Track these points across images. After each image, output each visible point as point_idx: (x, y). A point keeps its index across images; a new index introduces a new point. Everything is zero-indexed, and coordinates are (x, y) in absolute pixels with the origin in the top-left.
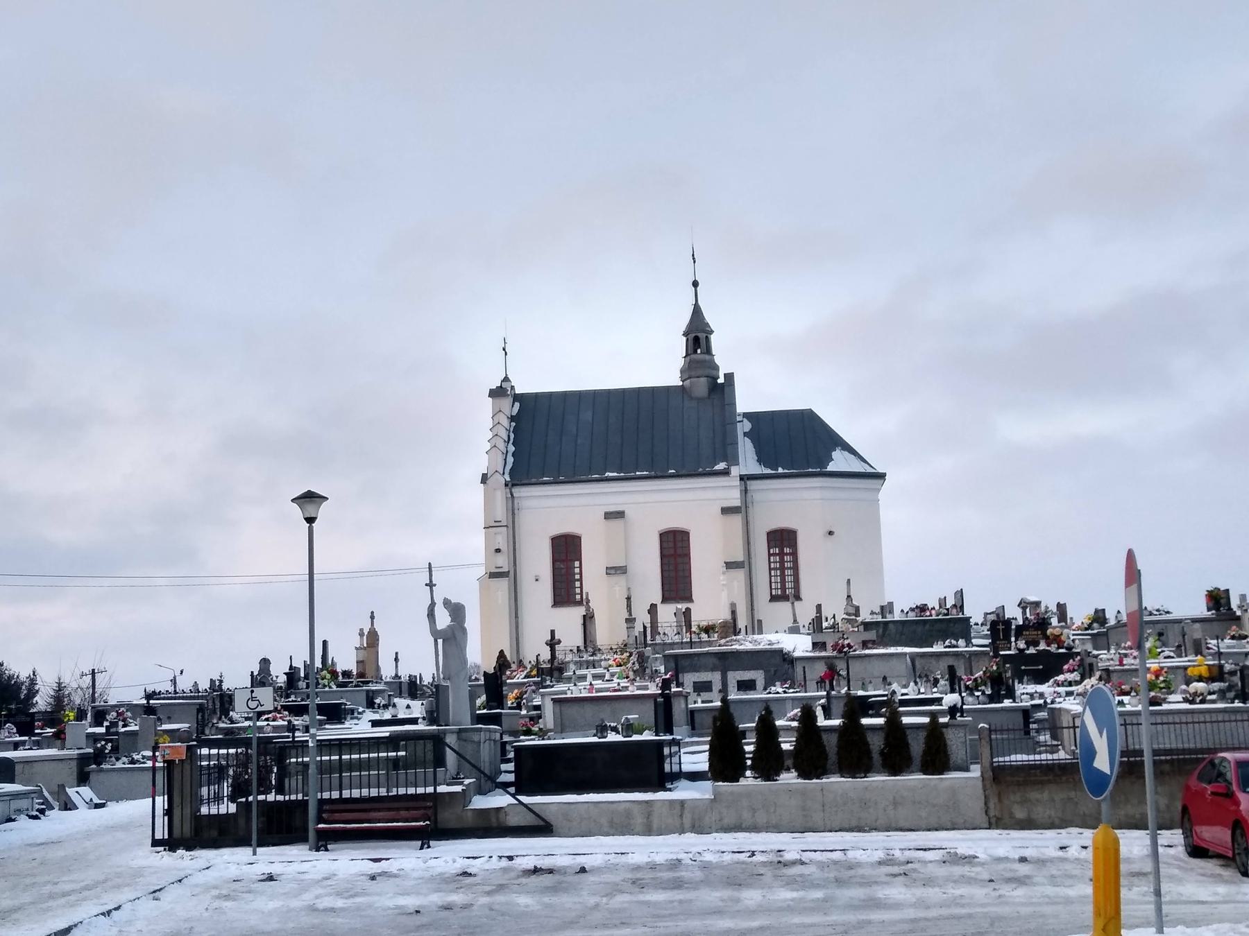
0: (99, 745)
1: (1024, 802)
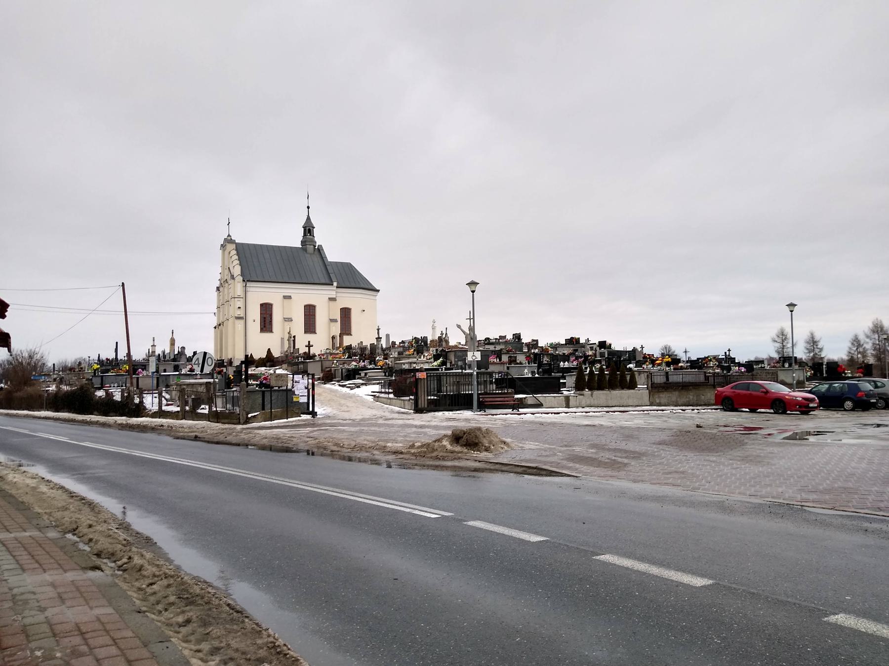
1: (659, 397)
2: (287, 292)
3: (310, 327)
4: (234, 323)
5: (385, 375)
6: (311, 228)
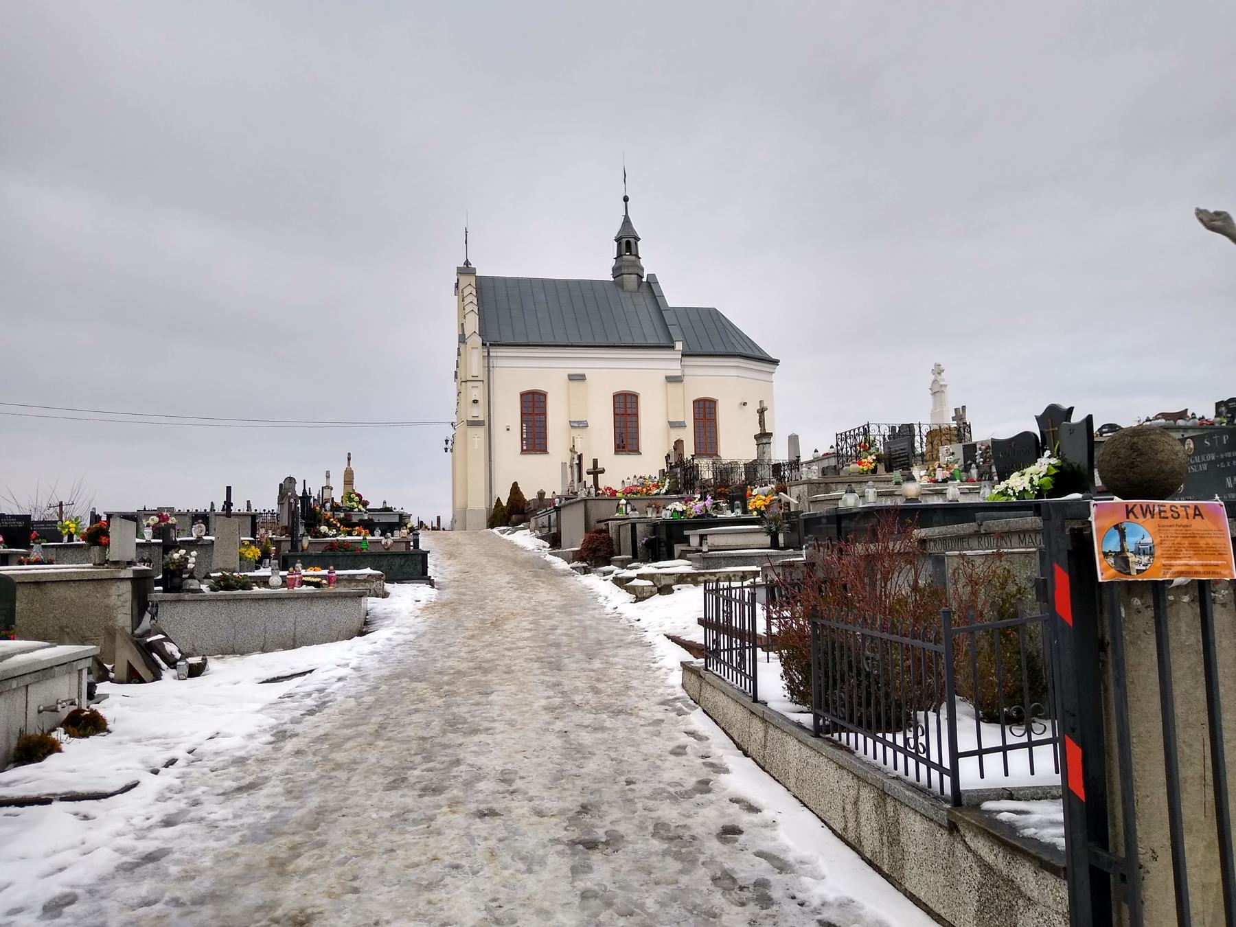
0: (176, 556)
2: (577, 367)
3: (626, 441)
4: (465, 434)
5: (774, 545)
6: (632, 240)
